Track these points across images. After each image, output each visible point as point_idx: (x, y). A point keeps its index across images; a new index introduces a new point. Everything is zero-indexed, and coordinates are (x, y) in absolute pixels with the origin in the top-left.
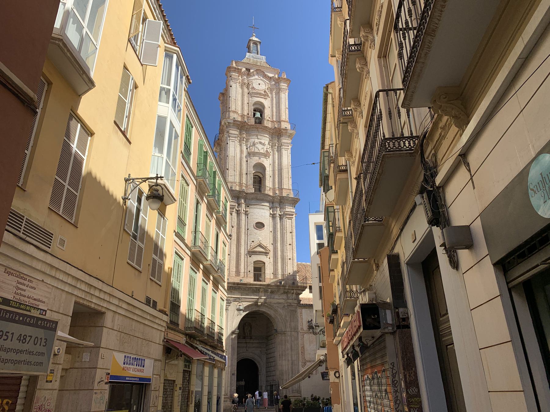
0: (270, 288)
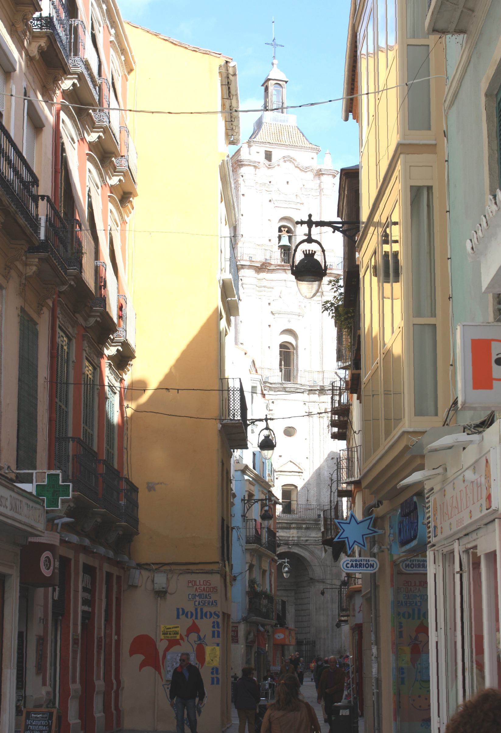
0: (304, 524)
